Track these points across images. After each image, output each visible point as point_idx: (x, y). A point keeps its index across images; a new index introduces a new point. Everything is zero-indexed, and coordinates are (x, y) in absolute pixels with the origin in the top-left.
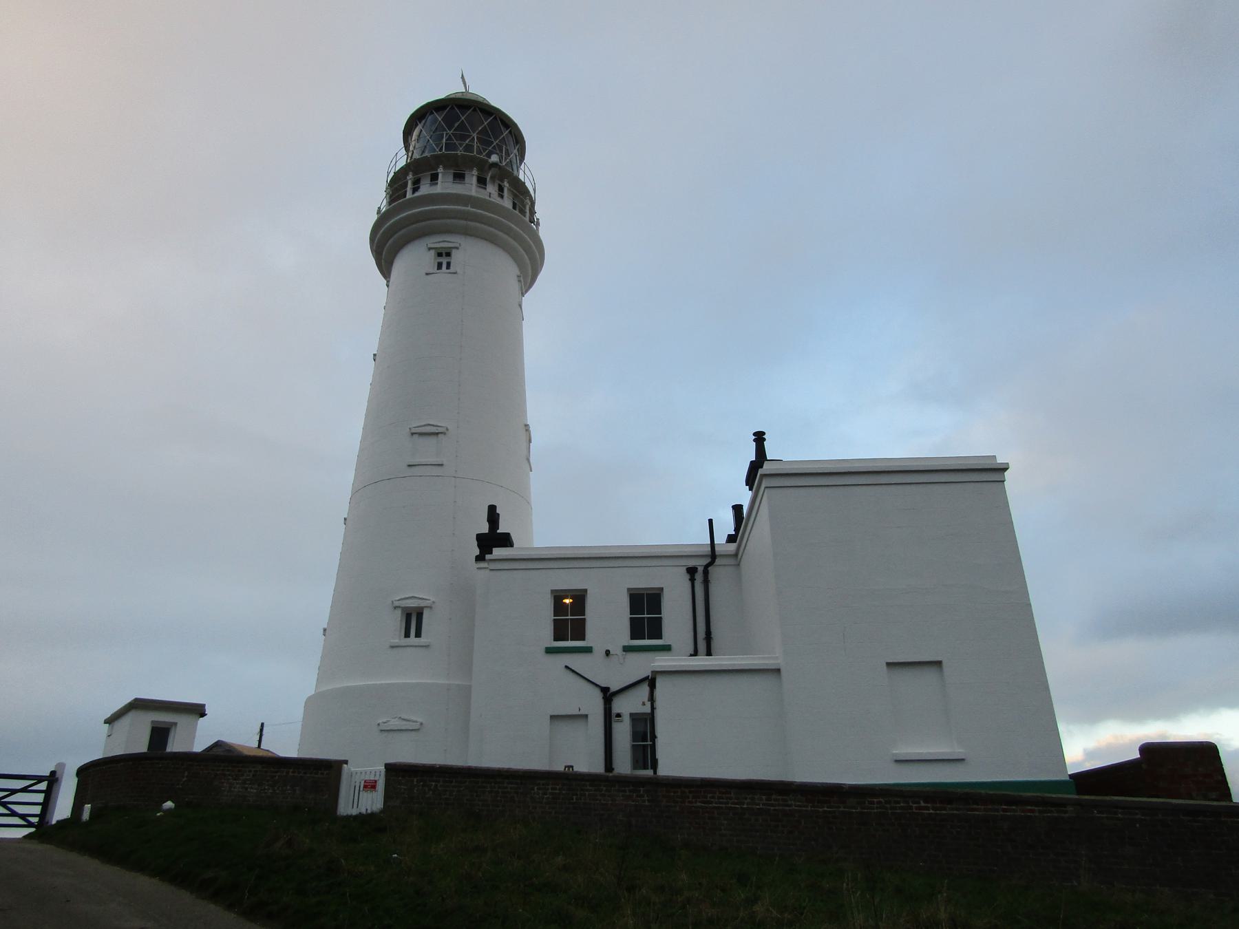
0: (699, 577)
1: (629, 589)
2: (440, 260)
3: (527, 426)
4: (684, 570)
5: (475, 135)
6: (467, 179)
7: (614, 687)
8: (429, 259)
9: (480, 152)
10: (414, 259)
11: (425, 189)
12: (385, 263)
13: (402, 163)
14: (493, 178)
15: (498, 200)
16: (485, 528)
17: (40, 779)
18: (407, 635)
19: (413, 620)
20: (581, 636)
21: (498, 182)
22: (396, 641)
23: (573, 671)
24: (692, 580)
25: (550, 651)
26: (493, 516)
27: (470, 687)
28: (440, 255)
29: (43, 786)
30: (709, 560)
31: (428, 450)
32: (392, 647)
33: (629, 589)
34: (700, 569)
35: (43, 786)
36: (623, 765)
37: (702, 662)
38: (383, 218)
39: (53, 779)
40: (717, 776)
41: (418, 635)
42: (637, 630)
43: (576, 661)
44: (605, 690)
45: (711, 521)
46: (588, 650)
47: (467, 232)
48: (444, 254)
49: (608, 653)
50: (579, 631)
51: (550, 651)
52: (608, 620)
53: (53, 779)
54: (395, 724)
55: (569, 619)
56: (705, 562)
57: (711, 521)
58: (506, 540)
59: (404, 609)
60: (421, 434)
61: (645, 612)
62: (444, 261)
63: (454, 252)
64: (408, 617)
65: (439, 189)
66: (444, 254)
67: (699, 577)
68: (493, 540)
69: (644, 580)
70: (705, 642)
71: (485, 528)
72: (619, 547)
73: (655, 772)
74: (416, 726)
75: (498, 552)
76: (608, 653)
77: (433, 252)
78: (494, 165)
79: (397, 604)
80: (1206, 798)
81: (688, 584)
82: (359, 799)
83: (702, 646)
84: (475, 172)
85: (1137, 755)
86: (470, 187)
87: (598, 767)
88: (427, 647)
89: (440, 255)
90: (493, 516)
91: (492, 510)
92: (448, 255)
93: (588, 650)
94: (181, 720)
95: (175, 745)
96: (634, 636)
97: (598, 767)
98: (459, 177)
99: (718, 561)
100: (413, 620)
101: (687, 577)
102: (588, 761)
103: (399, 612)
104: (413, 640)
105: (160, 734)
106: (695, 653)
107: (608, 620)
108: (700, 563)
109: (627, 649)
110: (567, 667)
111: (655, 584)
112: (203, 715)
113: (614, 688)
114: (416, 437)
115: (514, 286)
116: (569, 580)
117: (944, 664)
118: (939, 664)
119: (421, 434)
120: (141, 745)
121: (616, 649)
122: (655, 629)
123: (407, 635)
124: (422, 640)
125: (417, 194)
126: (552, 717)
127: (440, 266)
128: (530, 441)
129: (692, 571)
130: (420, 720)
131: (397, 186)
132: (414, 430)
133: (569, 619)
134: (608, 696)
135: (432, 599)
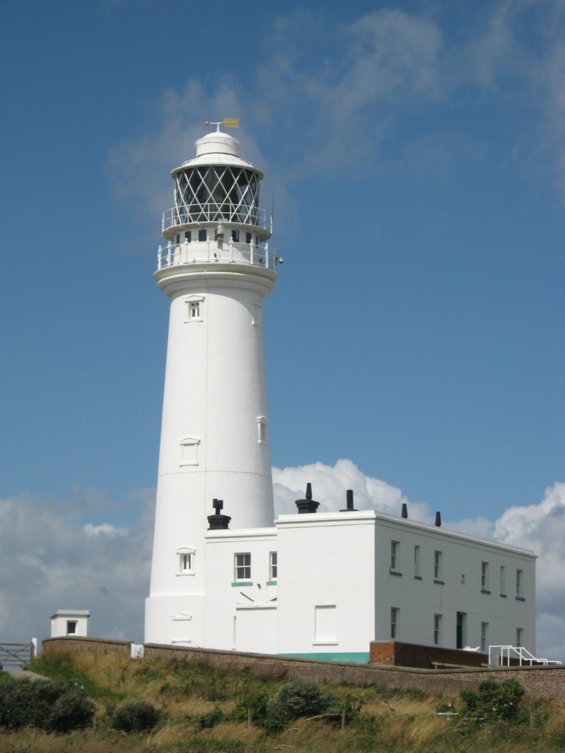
2: (193, 307)
20: (248, 576)
22: (178, 572)
28: (193, 305)
43: (245, 590)
45: (334, 606)
46: (251, 584)
48: (194, 305)
49: (259, 586)
51: (235, 585)
54: (179, 616)
57: (334, 606)
59: (181, 554)
60: (185, 445)
63: (200, 303)
66: (194, 305)
72: (292, 654)
74: (189, 618)
79: (178, 551)
92: (198, 304)
93: (251, 584)
103: (179, 556)
119: (185, 445)
123: (185, 568)
130: (191, 615)
135: (194, 548)
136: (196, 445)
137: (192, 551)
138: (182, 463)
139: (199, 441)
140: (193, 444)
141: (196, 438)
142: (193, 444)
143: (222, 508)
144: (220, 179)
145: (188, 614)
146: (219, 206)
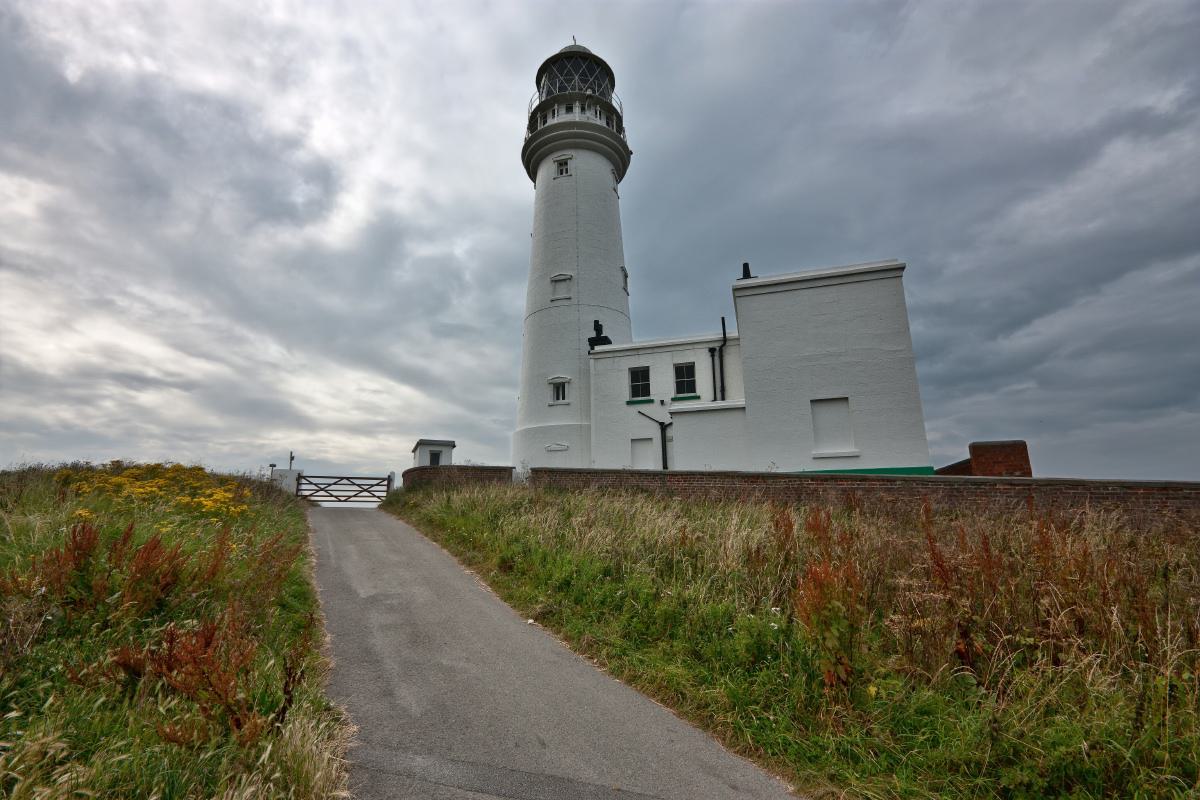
0: (717, 354)
3: (623, 269)
5: (577, 78)
8: (554, 167)
9: (581, 89)
11: (551, 122)
12: (532, 174)
13: (537, 103)
16: (593, 334)
17: (384, 480)
19: (559, 389)
24: (713, 356)
25: (629, 403)
26: (598, 327)
29: (386, 483)
31: (562, 291)
35: (386, 483)
37: (720, 404)
38: (528, 143)
39: (390, 479)
40: (491, 465)
41: (563, 398)
43: (644, 408)
44: (662, 424)
45: (723, 319)
47: (576, 147)
49: (662, 402)
50: (646, 391)
51: (629, 403)
52: (662, 383)
53: (390, 479)
54: (554, 447)
55: (640, 382)
56: (720, 344)
57: (723, 319)
58: (606, 341)
59: (554, 384)
61: (685, 378)
65: (555, 121)
67: (717, 354)
68: (599, 339)
69: (684, 358)
70: (720, 391)
71: (593, 334)
73: (665, 466)
75: (598, 348)
78: (590, 96)
80: (1012, 474)
81: (710, 359)
83: (719, 395)
88: (568, 404)
90: (598, 327)
92: (566, 164)
93: (652, 401)
94: (444, 450)
95: (443, 462)
96: (678, 392)
97: (659, 467)
98: (569, 109)
99: (727, 344)
100: (559, 389)
101: (709, 354)
104: (561, 401)
105: (435, 457)
106: (715, 399)
107: (662, 383)
111: (690, 360)
112: (454, 446)
116: (639, 362)
117: (850, 399)
118: (846, 399)
120: (427, 462)
121: (667, 400)
122: (691, 387)
124: (566, 401)
125: (546, 125)
126: (632, 440)
128: (626, 276)
129: (712, 351)
131: (537, 117)
133: (640, 382)
140: (564, 280)
142: (564, 280)
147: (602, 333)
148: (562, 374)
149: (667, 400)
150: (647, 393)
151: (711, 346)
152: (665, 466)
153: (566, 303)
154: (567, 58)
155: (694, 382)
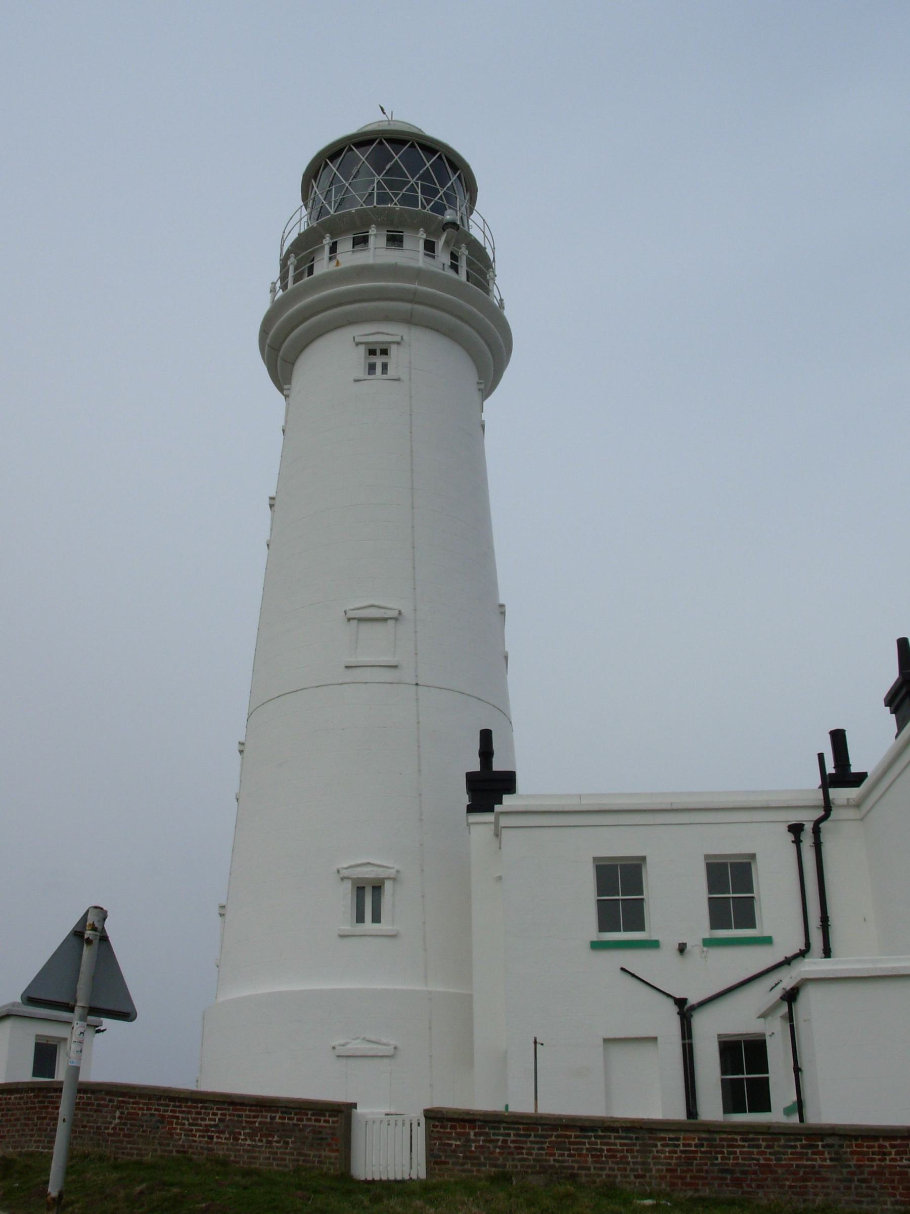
1: (707, 857)
2: (373, 359)
4: (784, 828)
6: (407, 243)
7: (693, 1000)
10: (333, 359)
14: (447, 243)
15: (451, 273)
16: (476, 767)
18: (360, 919)
19: (368, 895)
21: (452, 248)
23: (633, 975)
24: (797, 842)
27: (471, 996)
28: (372, 352)
30: (821, 813)
32: (341, 936)
33: (707, 857)
34: (809, 827)
36: (711, 1108)
41: (376, 918)
42: (720, 915)
43: (635, 960)
44: (680, 1003)
46: (653, 945)
47: (409, 320)
48: (377, 351)
50: (635, 917)
51: (597, 946)
52: (676, 900)
54: (357, 1046)
55: (620, 894)
59: (354, 881)
61: (730, 890)
62: (379, 360)
63: (393, 350)
64: (360, 891)
69: (730, 842)
71: (476, 767)
73: (802, 1119)
74: (389, 1051)
76: (682, 948)
77: (362, 350)
79: (345, 873)
82: (387, 1151)
84: (422, 235)
85: (505, 797)
86: (412, 254)
87: (679, 1113)
89: (372, 352)
91: (486, 737)
92: (385, 352)
93: (653, 945)
97: (679, 1113)
101: (791, 837)
102: (660, 1103)
103: (348, 885)
104: (368, 925)
107: (676, 900)
108: (808, 818)
109: (709, 943)
110: (623, 969)
113: (671, 1002)
114: (354, 623)
115: (477, 396)
116: (620, 845)
119: (360, 620)
121: (694, 942)
122: (745, 914)
123: (360, 919)
124: (384, 926)
126: (606, 1041)
127: (372, 368)
129: (796, 829)
130: (393, 1042)
131: (301, 255)
132: (351, 614)
133: (620, 894)
134: (685, 1011)
136: (391, 623)
137: (391, 873)
138: (352, 661)
139: (400, 613)
140: (385, 620)
141: (394, 604)
142: (385, 620)
143: (471, 778)
144: (428, 165)
145: (384, 1040)
146: (441, 198)
147: (495, 760)
148: (373, 860)
149: (694, 942)
150: (750, 922)
151: (795, 817)
152: (802, 1119)
153: (387, 675)
154: (391, 141)
155: (601, 890)
